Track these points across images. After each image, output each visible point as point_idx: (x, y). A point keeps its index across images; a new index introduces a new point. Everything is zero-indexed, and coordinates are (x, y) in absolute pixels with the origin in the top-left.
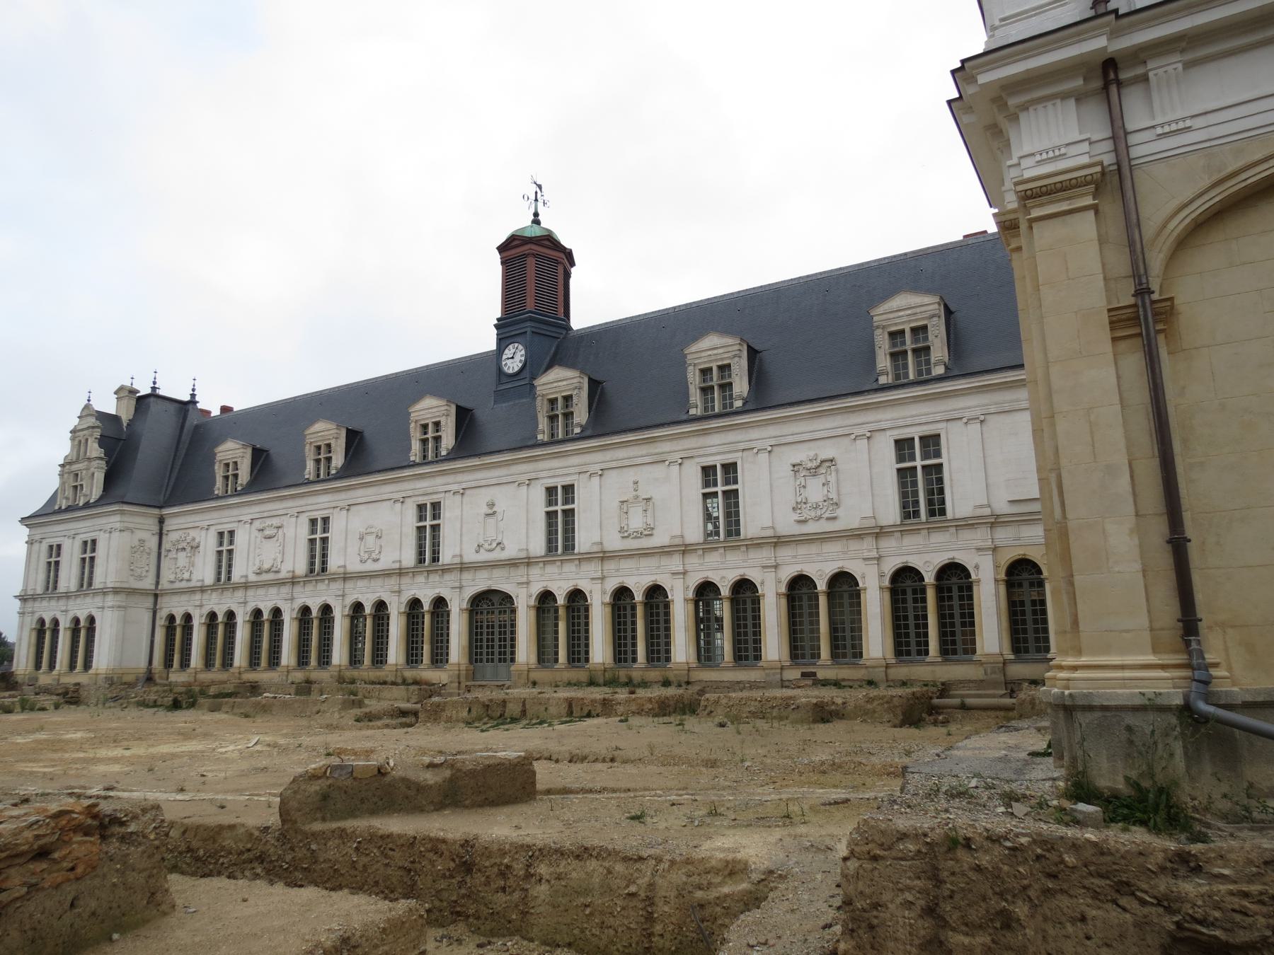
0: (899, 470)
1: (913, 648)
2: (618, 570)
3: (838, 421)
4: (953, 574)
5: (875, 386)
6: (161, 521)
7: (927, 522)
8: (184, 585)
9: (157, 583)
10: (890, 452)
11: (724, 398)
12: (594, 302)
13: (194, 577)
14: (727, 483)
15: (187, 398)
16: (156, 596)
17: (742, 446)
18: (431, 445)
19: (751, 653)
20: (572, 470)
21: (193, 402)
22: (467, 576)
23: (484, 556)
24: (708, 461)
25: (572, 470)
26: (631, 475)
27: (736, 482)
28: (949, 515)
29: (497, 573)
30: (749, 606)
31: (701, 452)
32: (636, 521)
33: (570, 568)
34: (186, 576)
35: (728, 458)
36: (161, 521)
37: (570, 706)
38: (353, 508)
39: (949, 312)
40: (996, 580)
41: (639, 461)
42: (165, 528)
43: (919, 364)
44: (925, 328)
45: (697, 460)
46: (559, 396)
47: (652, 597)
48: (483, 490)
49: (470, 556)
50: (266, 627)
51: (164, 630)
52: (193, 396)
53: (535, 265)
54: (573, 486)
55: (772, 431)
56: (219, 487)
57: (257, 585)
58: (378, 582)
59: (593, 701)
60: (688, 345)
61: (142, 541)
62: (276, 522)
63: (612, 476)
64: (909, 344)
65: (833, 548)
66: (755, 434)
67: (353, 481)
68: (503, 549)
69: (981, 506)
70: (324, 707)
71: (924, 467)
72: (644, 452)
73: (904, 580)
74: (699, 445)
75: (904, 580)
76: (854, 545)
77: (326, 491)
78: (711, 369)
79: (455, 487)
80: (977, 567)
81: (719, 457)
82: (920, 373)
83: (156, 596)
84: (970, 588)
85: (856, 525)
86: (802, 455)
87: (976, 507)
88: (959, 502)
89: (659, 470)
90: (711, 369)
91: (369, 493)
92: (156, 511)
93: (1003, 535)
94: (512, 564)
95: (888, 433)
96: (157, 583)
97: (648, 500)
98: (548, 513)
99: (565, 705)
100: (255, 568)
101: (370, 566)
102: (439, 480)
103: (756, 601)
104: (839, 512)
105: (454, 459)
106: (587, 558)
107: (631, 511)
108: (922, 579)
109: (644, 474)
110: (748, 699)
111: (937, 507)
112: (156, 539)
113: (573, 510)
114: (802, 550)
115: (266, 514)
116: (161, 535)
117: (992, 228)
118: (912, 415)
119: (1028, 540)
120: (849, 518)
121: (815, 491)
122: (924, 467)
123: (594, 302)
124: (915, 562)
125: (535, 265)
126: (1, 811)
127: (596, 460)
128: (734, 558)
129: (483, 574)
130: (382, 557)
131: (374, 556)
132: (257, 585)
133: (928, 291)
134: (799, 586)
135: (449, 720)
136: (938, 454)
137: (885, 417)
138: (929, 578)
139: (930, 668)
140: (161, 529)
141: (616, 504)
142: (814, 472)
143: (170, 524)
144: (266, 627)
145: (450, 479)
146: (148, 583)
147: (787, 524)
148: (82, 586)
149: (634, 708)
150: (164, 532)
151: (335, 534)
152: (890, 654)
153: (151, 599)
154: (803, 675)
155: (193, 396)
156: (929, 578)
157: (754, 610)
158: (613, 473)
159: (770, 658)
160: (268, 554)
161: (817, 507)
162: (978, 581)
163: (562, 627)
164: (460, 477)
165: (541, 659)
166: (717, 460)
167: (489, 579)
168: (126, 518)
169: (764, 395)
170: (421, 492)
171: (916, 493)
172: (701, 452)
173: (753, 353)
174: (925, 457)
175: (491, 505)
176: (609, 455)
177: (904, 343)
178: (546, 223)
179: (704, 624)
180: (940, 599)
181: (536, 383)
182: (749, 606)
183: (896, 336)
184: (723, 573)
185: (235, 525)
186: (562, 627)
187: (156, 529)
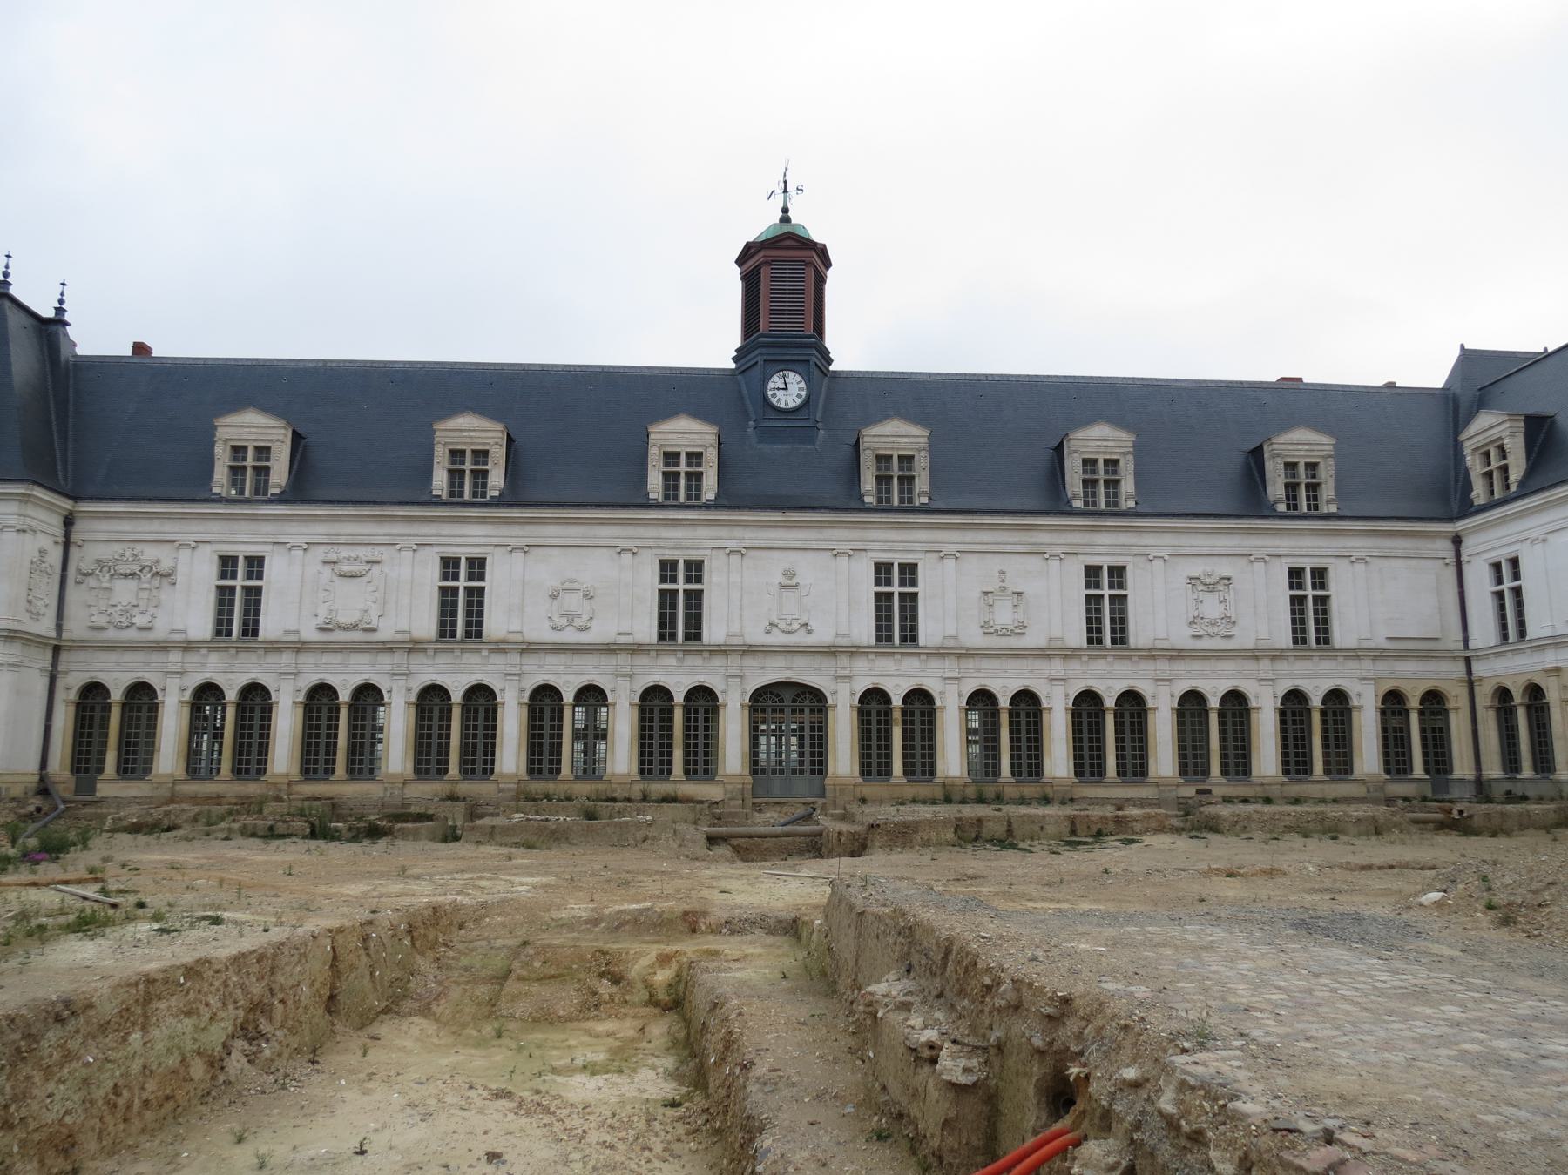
0: (218, 587)
1: (434, 766)
2: (979, 670)
3: (1235, 540)
4: (920, 699)
5: (858, 504)
6: (69, 522)
7: (461, 642)
8: (131, 634)
9: (59, 627)
10: (435, 570)
11: (258, 482)
12: (858, 337)
13: (158, 624)
14: (249, 576)
15: (50, 314)
16: (57, 650)
17: (1136, 550)
18: (1303, 493)
19: (254, 766)
20: (917, 547)
21: (59, 321)
22: (750, 662)
23: (777, 638)
24: (1095, 561)
25: (917, 547)
26: (996, 563)
27: (260, 577)
28: (922, 641)
29: (800, 661)
30: (257, 714)
31: (1088, 550)
32: (1004, 616)
33: (912, 663)
34: (140, 620)
35: (1117, 561)
36: (1457, 541)
37: (1073, 823)
38: (535, 551)
39: (510, 440)
40: (408, 703)
41: (1009, 548)
42: (75, 537)
43: (475, 485)
44: (1116, 462)
45: (1081, 557)
46: (895, 454)
47: (133, 698)
48: (776, 554)
49: (756, 636)
50: (1521, 715)
51: (1492, 714)
52: (60, 311)
53: (783, 276)
54: (1124, 568)
55: (1168, 539)
56: (1479, 494)
57: (325, 648)
58: (590, 660)
59: (1103, 819)
60: (871, 421)
61: (42, 552)
62: (364, 553)
63: (972, 563)
64: (250, 461)
65: (1228, 666)
66: (1149, 539)
67: (516, 513)
68: (810, 632)
69: (403, 632)
70: (652, 832)
71: (900, 594)
72: (1016, 540)
73: (655, 698)
74: (1085, 541)
75: (432, 698)
76: (1250, 665)
77: (483, 521)
78: (245, 448)
79: (732, 544)
80: (942, 693)
81: (242, 548)
82: (475, 494)
83: (57, 650)
84: (495, 711)
85: (721, 642)
86: (1197, 568)
87: (398, 632)
88: (1343, 634)
89: (1035, 561)
90: (245, 448)
91: (574, 533)
92: (67, 504)
93: (1382, 667)
94: (831, 652)
95: (1284, 560)
96: (1466, 641)
97: (1019, 594)
98: (878, 595)
99: (1067, 823)
100: (320, 621)
101: (570, 636)
102: (703, 532)
103: (267, 710)
104: (1234, 631)
105: (511, 505)
106: (500, 647)
107: (998, 603)
108: (449, 698)
109: (1014, 565)
110: (1282, 814)
111: (475, 629)
112: (59, 551)
113: (702, 591)
114: (1197, 665)
115: (343, 539)
116: (67, 545)
117: (832, 368)
118: (467, 535)
119: (1414, 679)
120: (1244, 638)
121: (1211, 607)
122: (900, 594)
123: (858, 337)
124: (1099, 687)
125: (783, 276)
126: (1567, 1027)
127: (952, 539)
128: (1123, 667)
129: (780, 662)
130: (594, 624)
131: (578, 622)
132: (325, 648)
133: (494, 416)
134: (1192, 702)
135: (926, 844)
136: (482, 577)
137: (1284, 544)
138: (679, 698)
139: (1320, 786)
140: (67, 535)
141: (976, 594)
142: (1211, 588)
143: (81, 530)
144: (1521, 715)
145: (723, 532)
146: (45, 627)
147: (1181, 637)
148: (1505, 637)
149: (1154, 825)
150: (1464, 557)
151: (496, 582)
152: (295, 769)
153: (49, 655)
154: (1199, 792)
155: (60, 311)
156: (679, 698)
157: (150, 718)
158: (974, 558)
159: (391, 770)
160: (350, 603)
161: (1213, 624)
162: (1050, 709)
163: (897, 733)
164: (738, 532)
165: (865, 771)
166: (1105, 561)
167: (790, 668)
168: (30, 510)
169: (301, 489)
170: (671, 543)
171: (231, 612)
172: (1088, 550)
173: (297, 438)
174: (902, 584)
175: (790, 574)
176: (969, 536)
177: (244, 459)
178: (795, 217)
179: (984, 739)
180: (465, 720)
181: (864, 432)
182: (257, 714)
183: (1089, 463)
184: (1110, 682)
185: (268, 548)
186: (897, 733)
187: (1450, 555)
